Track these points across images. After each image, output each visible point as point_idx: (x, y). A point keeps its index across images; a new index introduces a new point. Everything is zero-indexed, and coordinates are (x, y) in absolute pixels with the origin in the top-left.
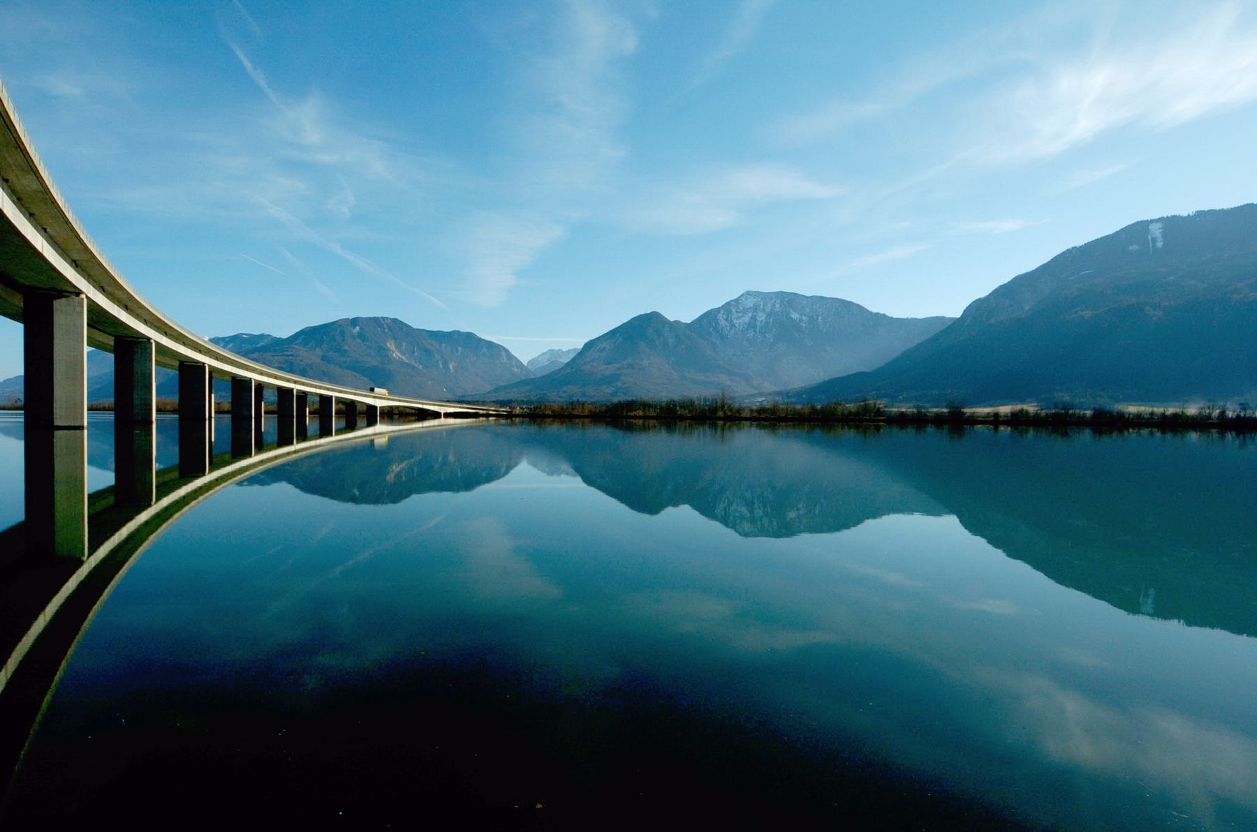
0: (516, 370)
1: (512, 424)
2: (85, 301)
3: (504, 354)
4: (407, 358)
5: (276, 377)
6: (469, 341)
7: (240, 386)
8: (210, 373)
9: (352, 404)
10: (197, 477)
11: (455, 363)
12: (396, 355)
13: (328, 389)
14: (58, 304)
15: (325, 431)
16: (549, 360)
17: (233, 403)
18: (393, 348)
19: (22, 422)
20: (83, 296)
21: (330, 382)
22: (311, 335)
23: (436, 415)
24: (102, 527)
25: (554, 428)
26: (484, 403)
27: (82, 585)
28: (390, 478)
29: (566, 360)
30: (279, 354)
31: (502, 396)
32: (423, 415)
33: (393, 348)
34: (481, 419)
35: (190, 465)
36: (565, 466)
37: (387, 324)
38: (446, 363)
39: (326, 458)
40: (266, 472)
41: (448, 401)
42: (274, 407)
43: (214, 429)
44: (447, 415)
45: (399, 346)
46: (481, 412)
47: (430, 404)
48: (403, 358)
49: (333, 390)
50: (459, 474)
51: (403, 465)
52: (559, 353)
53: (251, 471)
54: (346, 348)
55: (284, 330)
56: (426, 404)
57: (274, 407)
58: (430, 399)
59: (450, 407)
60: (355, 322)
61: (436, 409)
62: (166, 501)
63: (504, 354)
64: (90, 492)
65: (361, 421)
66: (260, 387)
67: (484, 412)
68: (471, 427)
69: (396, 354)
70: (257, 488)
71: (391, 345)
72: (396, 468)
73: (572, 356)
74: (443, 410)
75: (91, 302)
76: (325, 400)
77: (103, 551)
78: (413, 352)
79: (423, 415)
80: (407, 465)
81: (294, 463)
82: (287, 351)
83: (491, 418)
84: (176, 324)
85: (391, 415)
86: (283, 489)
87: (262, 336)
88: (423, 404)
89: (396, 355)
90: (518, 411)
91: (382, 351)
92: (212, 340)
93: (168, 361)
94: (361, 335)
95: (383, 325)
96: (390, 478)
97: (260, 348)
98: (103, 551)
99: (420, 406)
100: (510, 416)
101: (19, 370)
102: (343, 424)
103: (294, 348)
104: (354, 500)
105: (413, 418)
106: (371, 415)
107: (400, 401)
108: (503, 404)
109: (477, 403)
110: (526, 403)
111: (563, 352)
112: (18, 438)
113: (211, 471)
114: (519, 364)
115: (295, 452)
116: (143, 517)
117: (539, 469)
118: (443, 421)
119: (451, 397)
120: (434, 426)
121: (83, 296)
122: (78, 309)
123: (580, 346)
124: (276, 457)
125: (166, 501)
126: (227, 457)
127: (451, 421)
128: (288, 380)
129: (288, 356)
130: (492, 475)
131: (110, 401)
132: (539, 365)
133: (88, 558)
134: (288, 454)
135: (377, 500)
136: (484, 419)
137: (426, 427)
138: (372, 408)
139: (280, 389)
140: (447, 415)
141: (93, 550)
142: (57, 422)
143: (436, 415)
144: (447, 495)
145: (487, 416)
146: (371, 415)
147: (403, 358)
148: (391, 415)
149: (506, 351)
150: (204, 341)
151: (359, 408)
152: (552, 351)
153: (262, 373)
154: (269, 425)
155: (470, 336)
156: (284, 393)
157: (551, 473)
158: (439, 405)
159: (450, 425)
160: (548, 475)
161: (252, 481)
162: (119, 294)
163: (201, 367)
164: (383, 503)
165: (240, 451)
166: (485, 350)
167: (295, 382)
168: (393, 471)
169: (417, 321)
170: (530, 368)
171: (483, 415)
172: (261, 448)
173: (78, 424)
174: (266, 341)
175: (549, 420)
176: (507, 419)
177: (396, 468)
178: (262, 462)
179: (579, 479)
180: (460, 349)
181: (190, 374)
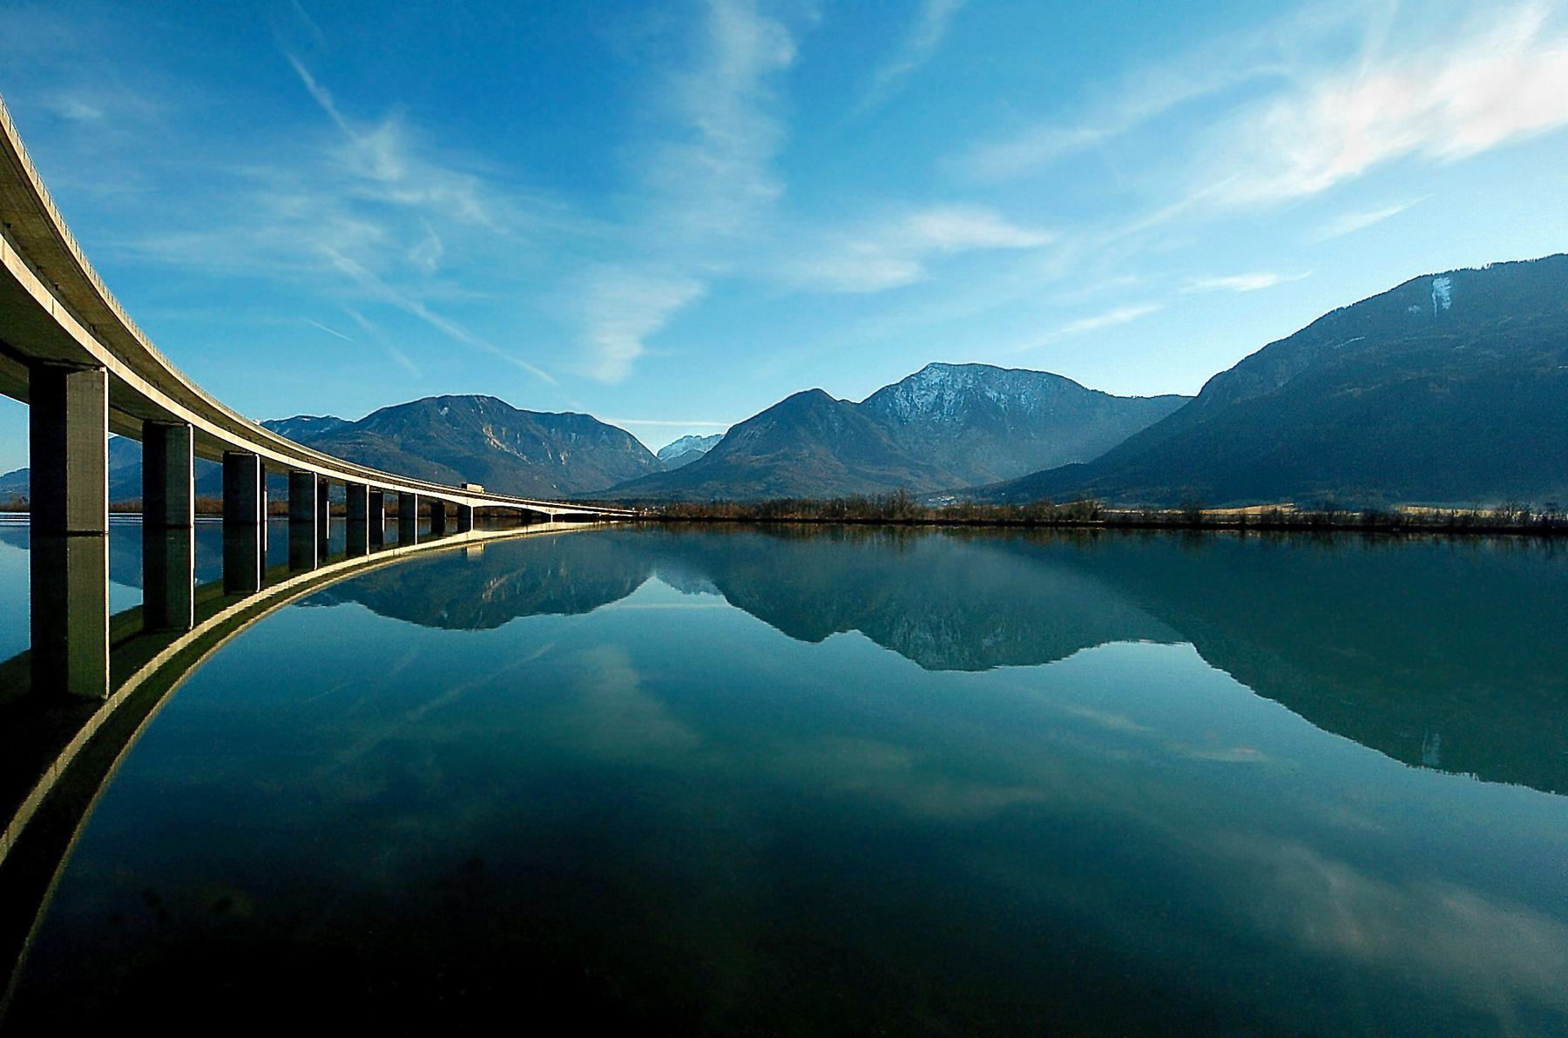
1: (639, 529)
4: (507, 447)
6: (584, 425)
7: (298, 481)
14: (71, 379)
15: (406, 539)
22: (387, 419)
23: (544, 518)
24: (128, 656)
25: (692, 535)
28: (487, 596)
31: (627, 494)
35: (237, 582)
36: (703, 582)
38: (556, 455)
39: (406, 571)
40: (332, 589)
41: (559, 501)
43: (265, 534)
44: (558, 518)
45: (497, 433)
48: (504, 446)
49: (415, 487)
51: (503, 580)
55: (354, 412)
60: (443, 401)
62: (206, 626)
63: (628, 440)
66: (325, 483)
71: (488, 431)
72: (494, 584)
73: (713, 444)
74: (552, 512)
76: (406, 499)
79: (528, 518)
82: (359, 438)
85: (486, 518)
86: (354, 609)
89: (494, 442)
91: (478, 438)
93: (209, 450)
94: (450, 418)
96: (487, 596)
98: (128, 688)
99: (524, 506)
104: (443, 624)
106: (463, 518)
108: (627, 504)
115: (369, 563)
116: (179, 645)
118: (552, 525)
119: (564, 496)
125: (206, 626)
126: (284, 569)
127: (563, 525)
129: (360, 444)
133: (109, 696)
134: (360, 566)
138: (464, 509)
140: (558, 518)
141: (116, 686)
142: (71, 527)
143: (544, 518)
144: (541, 616)
145: (608, 518)
146: (463, 518)
148: (486, 518)
154: (335, 530)
156: (354, 490)
157: (687, 591)
161: (315, 599)
165: (299, 563)
167: (368, 477)
169: (520, 400)
171: (603, 518)
177: (494, 584)
179: (722, 597)
181: (236, 466)
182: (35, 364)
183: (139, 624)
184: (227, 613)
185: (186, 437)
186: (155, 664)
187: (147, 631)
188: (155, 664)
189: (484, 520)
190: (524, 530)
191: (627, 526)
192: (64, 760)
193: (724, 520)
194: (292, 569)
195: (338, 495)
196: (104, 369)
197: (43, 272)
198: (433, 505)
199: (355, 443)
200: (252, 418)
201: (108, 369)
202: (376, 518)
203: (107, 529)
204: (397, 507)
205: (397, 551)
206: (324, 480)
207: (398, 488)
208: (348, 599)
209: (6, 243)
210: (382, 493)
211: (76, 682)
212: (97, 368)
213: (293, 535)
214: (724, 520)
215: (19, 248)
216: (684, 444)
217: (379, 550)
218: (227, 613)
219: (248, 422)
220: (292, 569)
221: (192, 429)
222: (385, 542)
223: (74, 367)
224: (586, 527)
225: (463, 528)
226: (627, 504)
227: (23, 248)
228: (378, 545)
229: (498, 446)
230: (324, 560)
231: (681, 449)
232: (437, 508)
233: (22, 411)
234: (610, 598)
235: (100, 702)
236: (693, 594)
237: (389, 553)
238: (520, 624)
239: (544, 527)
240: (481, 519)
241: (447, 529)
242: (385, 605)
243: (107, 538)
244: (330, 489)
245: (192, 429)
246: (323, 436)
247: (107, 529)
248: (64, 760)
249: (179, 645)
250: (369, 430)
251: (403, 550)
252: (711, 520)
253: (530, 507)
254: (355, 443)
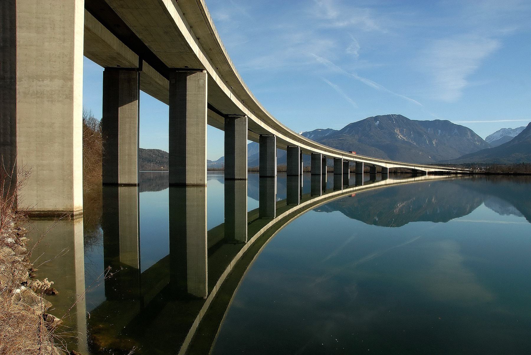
0: (478, 143)
1: (473, 179)
2: (247, 118)
3: (469, 133)
4: (406, 138)
5: (333, 152)
6: (446, 125)
7: (315, 157)
8: (301, 151)
9: (373, 167)
10: (296, 206)
11: (437, 140)
12: (400, 137)
13: (360, 158)
14: (236, 121)
15: (358, 183)
16: (501, 135)
17: (312, 168)
18: (398, 132)
19: (167, 173)
20: (246, 116)
21: (363, 155)
22: (352, 128)
23: (423, 173)
24: (254, 228)
25: (505, 183)
26: (454, 166)
27: (245, 254)
28: (396, 211)
29: (514, 135)
30: (336, 139)
31: (468, 161)
32: (415, 173)
33: (398, 132)
34: (452, 176)
35: (291, 201)
36: (512, 208)
37: (395, 119)
38: (431, 142)
39: (360, 196)
40: (329, 204)
41: (432, 165)
42: (332, 169)
43: (303, 181)
44: (430, 173)
45: (401, 132)
46: (452, 171)
47: (419, 167)
48: (405, 138)
49: (363, 159)
50: (438, 211)
51: (404, 204)
52: (510, 130)
53: (320, 204)
54: (372, 134)
55: (338, 126)
56: (417, 166)
57: (332, 169)
58: (421, 163)
59: (432, 168)
60: (377, 118)
61: (423, 169)
62: (280, 217)
63: (469, 133)
64: (248, 211)
65: (378, 176)
66: (325, 158)
67: (454, 171)
68: (446, 181)
69: (400, 136)
70: (324, 213)
71: (397, 131)
72: (400, 205)
73: (519, 132)
74: (427, 170)
75: (250, 119)
76: (358, 164)
77: (253, 239)
78: (410, 135)
79: (415, 173)
80: (406, 204)
81: (344, 200)
82: (341, 137)
83: (459, 175)
84: (285, 127)
85: (395, 173)
86: (338, 215)
87: (328, 130)
88: (415, 166)
89: (400, 137)
90: (477, 170)
91: (393, 135)
92: (304, 134)
93: (282, 145)
94: (380, 126)
95: (392, 119)
96: (396, 211)
97: (326, 136)
98: (253, 239)
99: (413, 168)
100: (471, 174)
101: (222, 154)
102: (368, 179)
103: (344, 136)
104: (375, 223)
105: (409, 175)
106: (384, 173)
107: (401, 165)
108: (468, 166)
109: (448, 165)
110: (484, 165)
111: (512, 130)
112: (222, 182)
113: (301, 203)
114: (480, 139)
115: (342, 194)
116: (270, 224)
117: (493, 210)
118: (427, 177)
119: (434, 162)
120: (422, 180)
121: (246, 117)
122: (244, 123)
123: (526, 125)
124: (332, 197)
125: (280, 217)
126: (309, 195)
127: (433, 177)
128: (339, 154)
129: (341, 140)
130: (462, 212)
131: (257, 167)
132: (494, 140)
133: (247, 242)
134: (339, 195)
135: (387, 224)
136: (454, 176)
137: (417, 181)
138: (384, 169)
139: (335, 158)
140: (430, 173)
141: (250, 236)
142: (236, 177)
143: (423, 173)
144: (430, 223)
145: (456, 173)
146: (384, 173)
147: (405, 138)
148: (395, 173)
149: (471, 131)
150: (298, 134)
151: (377, 169)
152: (504, 130)
153: (325, 150)
154: (329, 179)
155: (446, 122)
156: (337, 161)
157: (502, 213)
158: (424, 167)
159: (432, 179)
160: (500, 214)
161: (323, 209)
162: (260, 114)
163: (296, 148)
164: (391, 226)
165: (315, 193)
166: (456, 131)
167: (343, 155)
168: (398, 207)
169: (412, 116)
170: (487, 141)
171: (453, 173)
172: (325, 192)
173: (199, 182)
174: (330, 132)
175: (500, 176)
176: (469, 176)
177: (400, 205)
178: (325, 199)
179: (524, 218)
180: (439, 131)
181: (291, 150)
182: (226, 116)
183: (257, 215)
184: (287, 213)
185: (273, 141)
186: (262, 231)
187: (260, 218)
188: (262, 231)
189: (394, 174)
190: (413, 179)
191: (467, 177)
192: (233, 263)
193: (523, 174)
194: (312, 196)
195: (331, 163)
196: (246, 116)
197: (227, 83)
198: (371, 167)
199: (339, 140)
200: (299, 132)
201: (247, 116)
202: (346, 174)
203: (247, 178)
204: (355, 168)
205: (355, 188)
206: (325, 157)
207: (355, 159)
208: (335, 209)
209: (231, 93)
210: (348, 162)
211: (237, 237)
212: (244, 116)
213: (312, 181)
214: (523, 174)
215: (221, 76)
216: (501, 133)
217: (347, 188)
218: (287, 213)
219: (295, 133)
220: (312, 196)
221: (275, 137)
222: (349, 184)
223: (193, 71)
224: (445, 178)
225: (384, 178)
226: (468, 166)
227: (222, 76)
228: (347, 185)
229: (402, 138)
230: (325, 192)
231: (499, 136)
232: (373, 168)
233: (222, 133)
234: (459, 215)
235: (244, 244)
236: (505, 215)
237: (351, 189)
238: (412, 226)
239: (423, 178)
240: (393, 174)
241: (377, 178)
242: (351, 213)
243: (247, 181)
244: (327, 160)
245: (275, 137)
246: (326, 137)
247: (247, 178)
248: (233, 263)
249: (270, 224)
250: (345, 133)
251: (357, 188)
252: (516, 174)
253: (416, 168)
254: (339, 140)
